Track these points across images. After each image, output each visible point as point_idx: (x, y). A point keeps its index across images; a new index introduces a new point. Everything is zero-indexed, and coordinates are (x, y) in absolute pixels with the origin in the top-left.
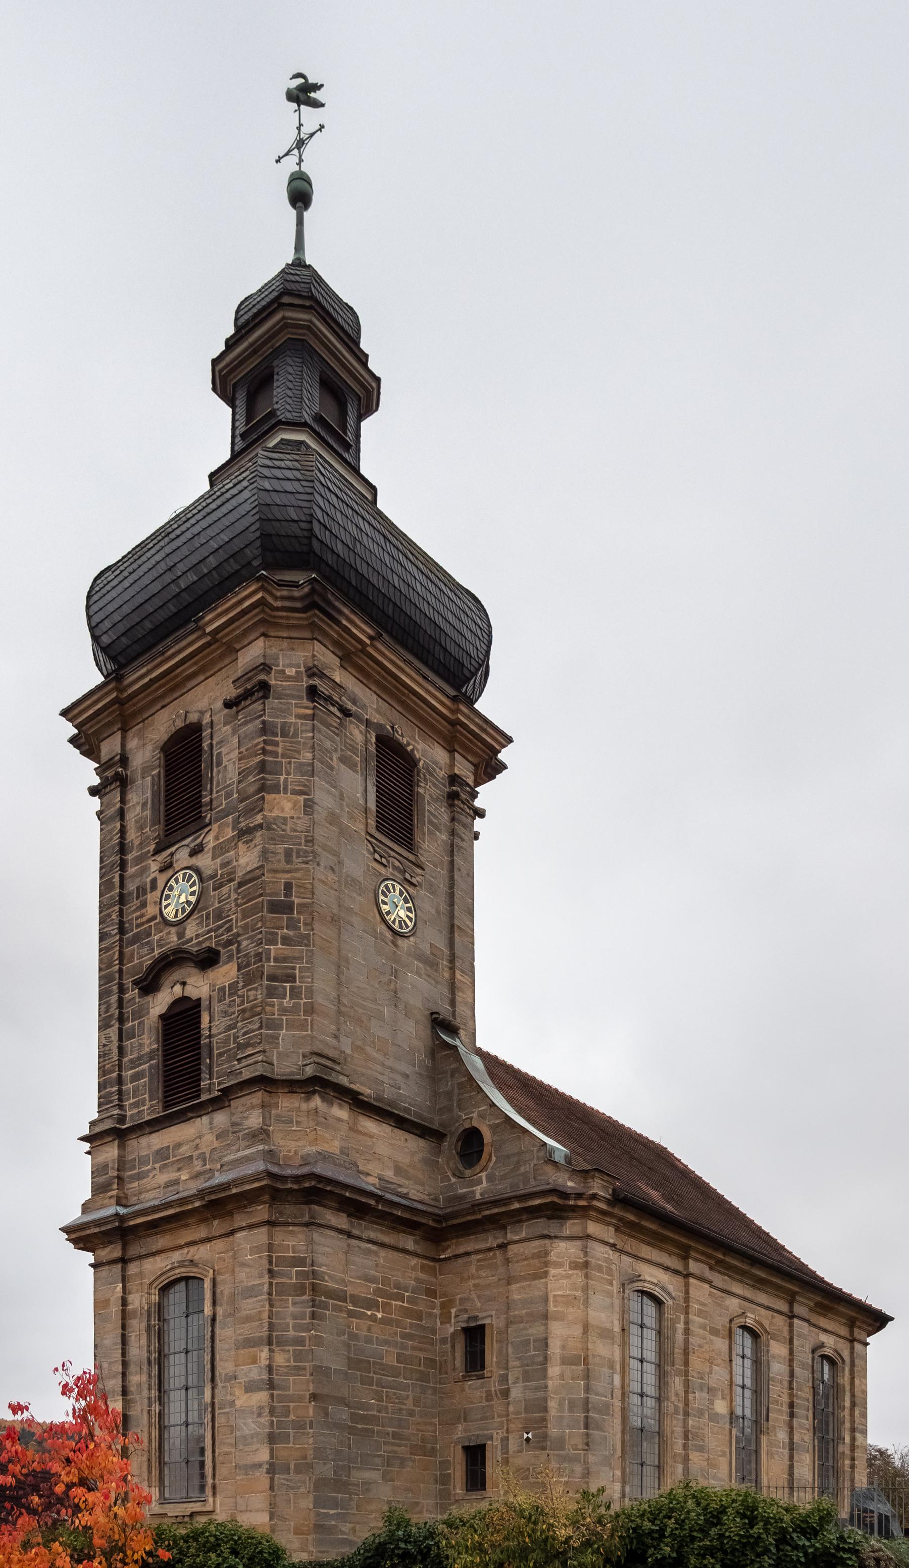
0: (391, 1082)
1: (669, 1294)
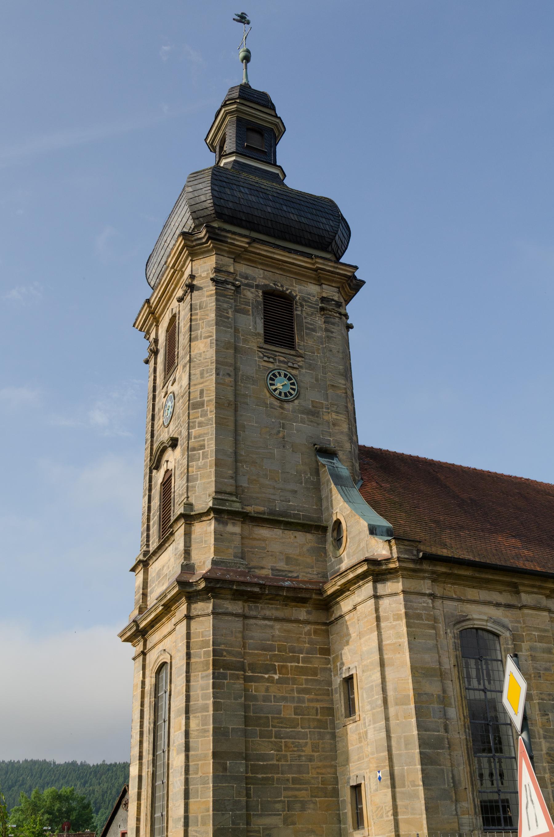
0: (282, 498)
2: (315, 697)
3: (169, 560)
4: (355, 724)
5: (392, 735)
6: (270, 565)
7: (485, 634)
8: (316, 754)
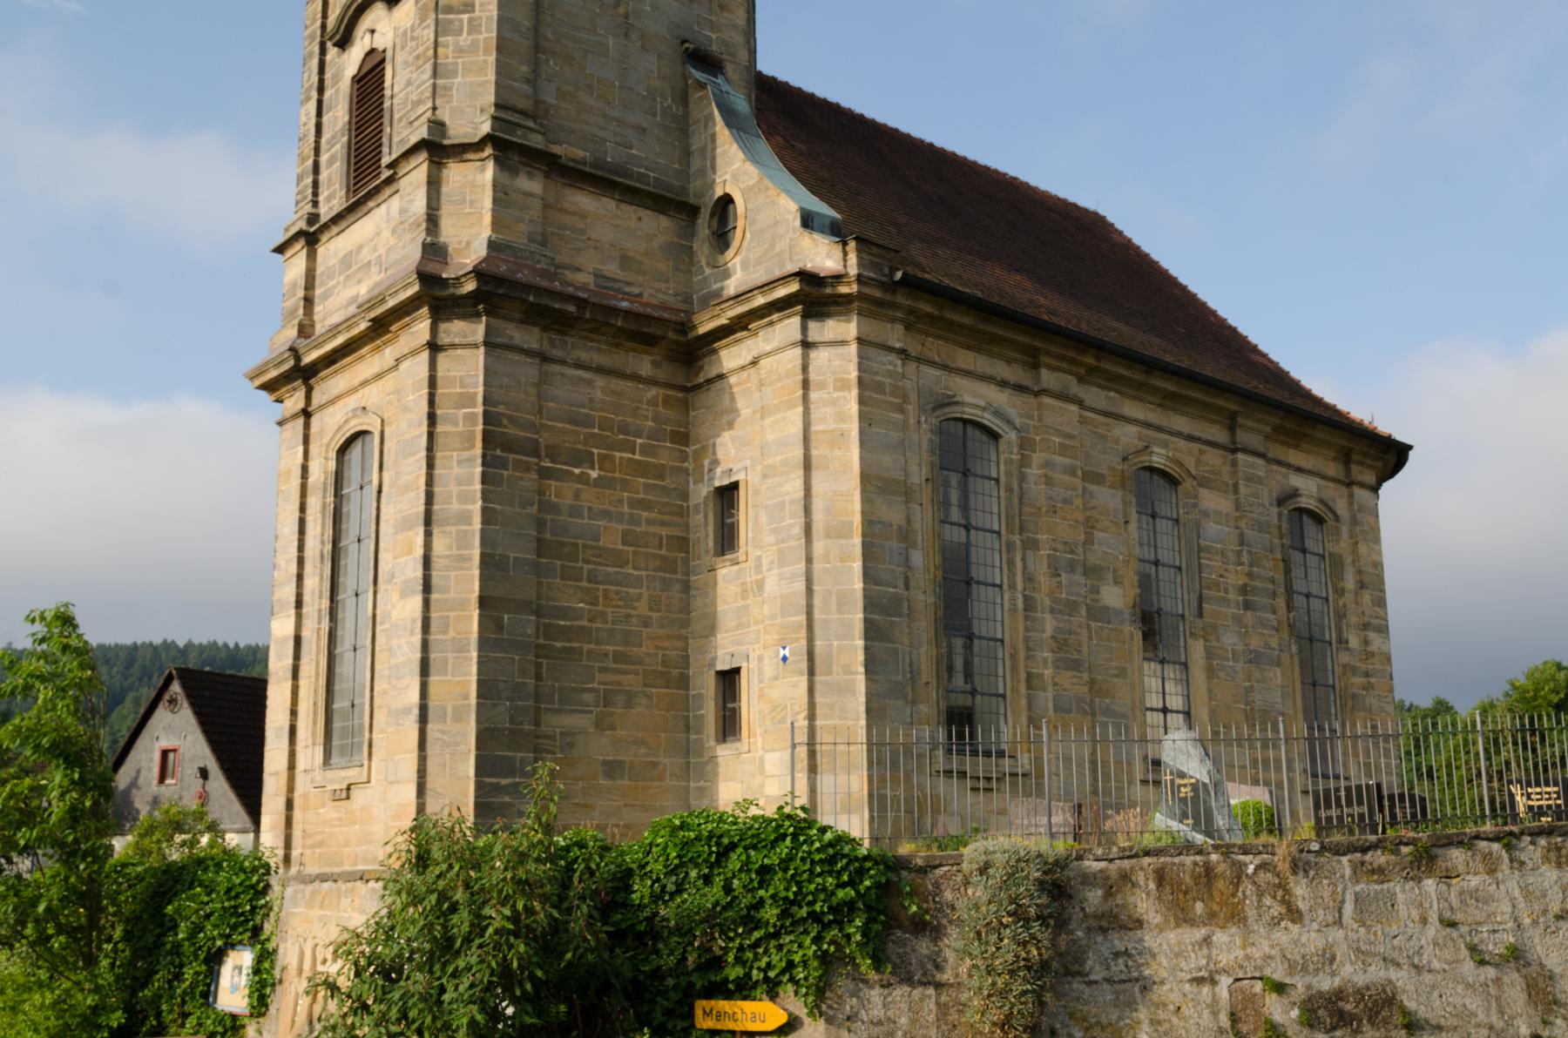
1: (1009, 422)
2: (659, 517)
3: (378, 234)
4: (735, 568)
5: (816, 588)
6: (591, 266)
7: (977, 433)
8: (655, 615)
